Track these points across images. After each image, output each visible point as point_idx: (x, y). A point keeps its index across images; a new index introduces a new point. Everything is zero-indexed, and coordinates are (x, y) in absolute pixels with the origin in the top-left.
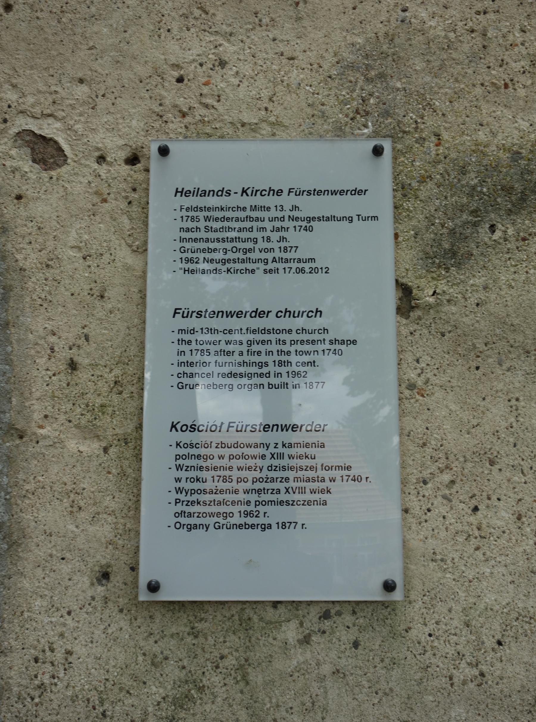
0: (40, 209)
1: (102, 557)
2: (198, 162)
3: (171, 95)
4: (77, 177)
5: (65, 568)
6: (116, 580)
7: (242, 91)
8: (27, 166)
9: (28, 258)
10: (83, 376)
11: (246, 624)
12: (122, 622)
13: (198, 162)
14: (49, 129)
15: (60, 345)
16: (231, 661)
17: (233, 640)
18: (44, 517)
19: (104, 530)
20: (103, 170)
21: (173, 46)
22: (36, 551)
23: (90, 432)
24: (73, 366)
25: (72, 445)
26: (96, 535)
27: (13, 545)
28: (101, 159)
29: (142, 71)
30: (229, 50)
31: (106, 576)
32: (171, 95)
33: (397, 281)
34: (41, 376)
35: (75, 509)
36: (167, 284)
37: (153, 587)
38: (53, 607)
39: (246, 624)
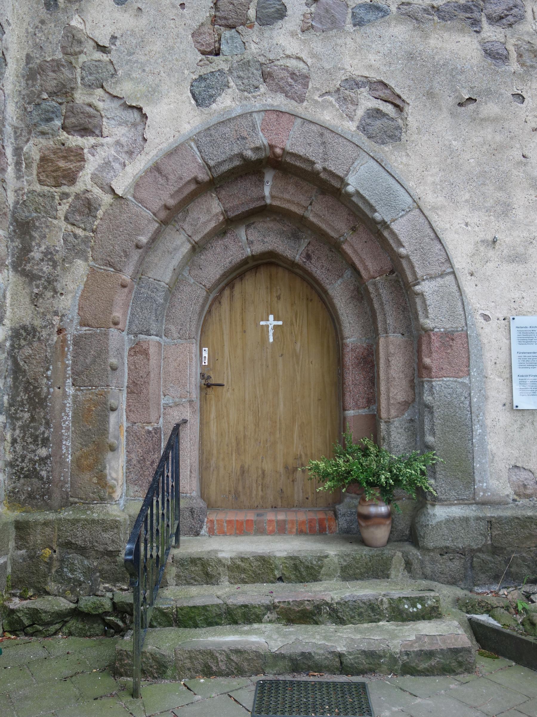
0: (486, 330)
1: (504, 401)
2: (520, 321)
3: (513, 305)
4: (493, 323)
5: (497, 404)
6: (507, 406)
7: (528, 304)
8: (483, 321)
9: (485, 341)
10: (498, 365)
11: (533, 414)
12: (508, 413)
13: (520, 321)
14: (487, 313)
15: (493, 359)
16: (530, 421)
17: (531, 417)
18: (492, 393)
19: (504, 396)
20: (499, 321)
21: (512, 294)
22: (491, 400)
23: (500, 377)
24: (495, 363)
25: (497, 379)
26: (503, 397)
27: (486, 399)
28: (498, 319)
29: (506, 300)
30: (524, 294)
31: (504, 405)
32: (513, 305)
33: (485, 51)
34: (489, 365)
35: (499, 392)
36: (516, 348)
37: (517, 407)
38: (494, 411)
39: (533, 414)
